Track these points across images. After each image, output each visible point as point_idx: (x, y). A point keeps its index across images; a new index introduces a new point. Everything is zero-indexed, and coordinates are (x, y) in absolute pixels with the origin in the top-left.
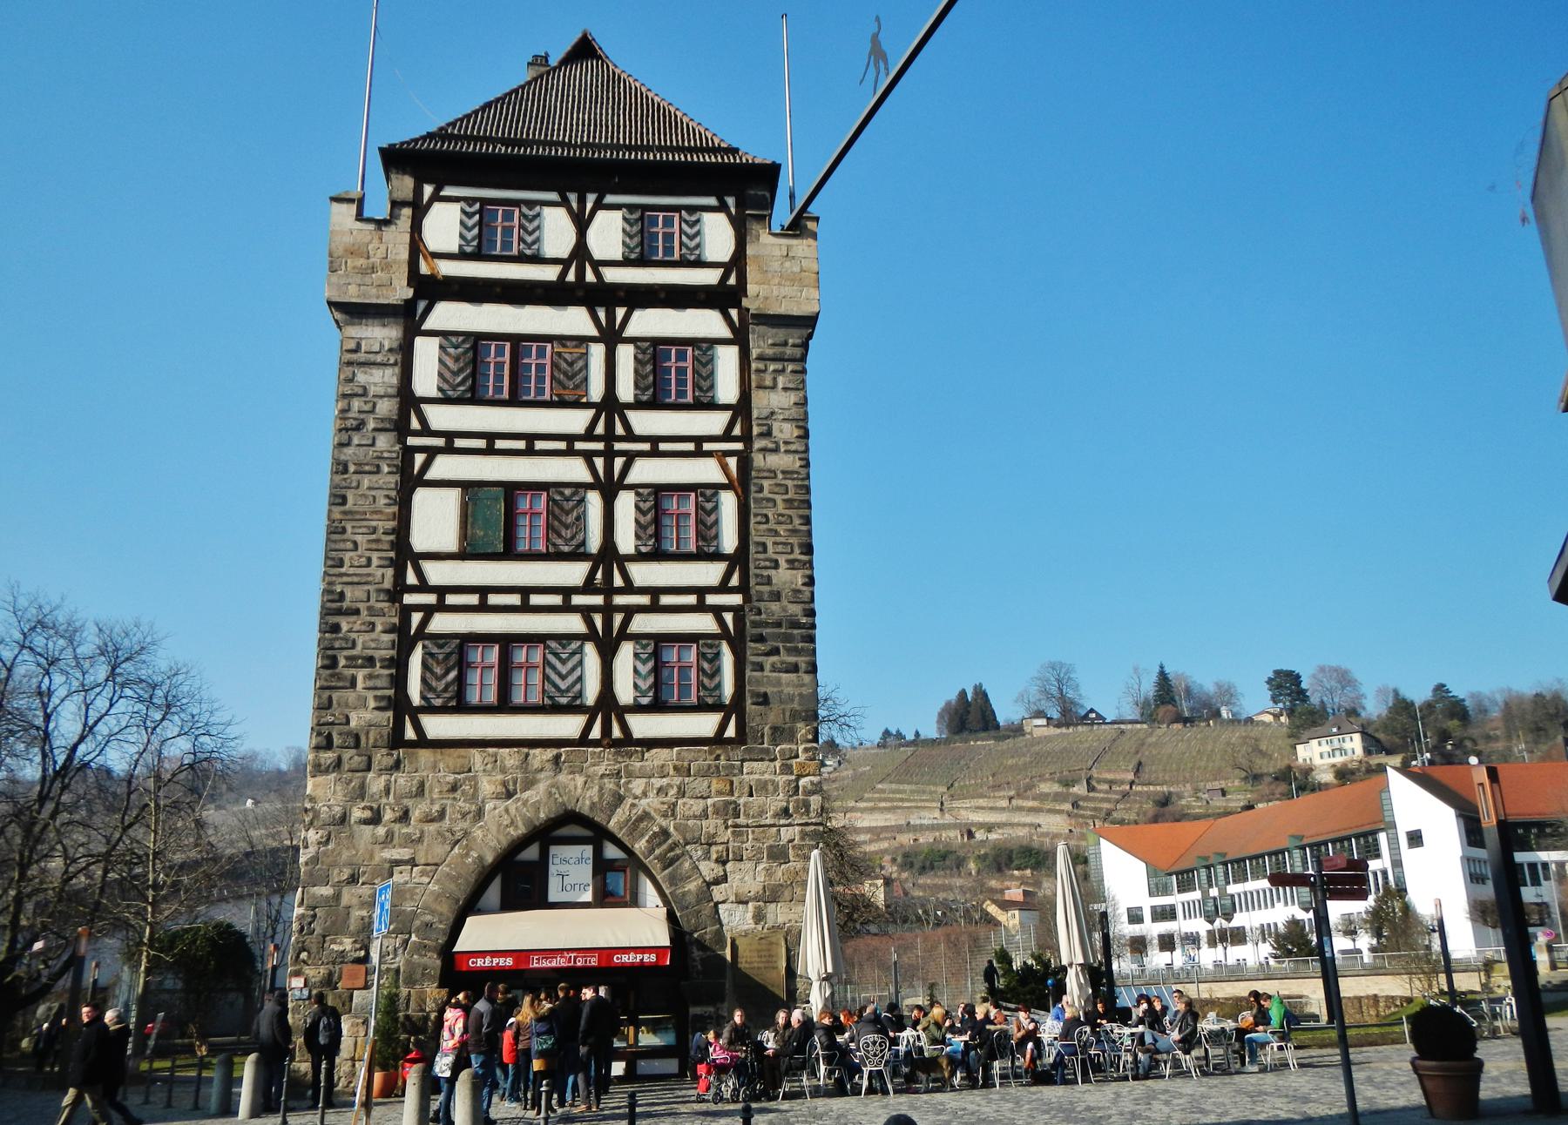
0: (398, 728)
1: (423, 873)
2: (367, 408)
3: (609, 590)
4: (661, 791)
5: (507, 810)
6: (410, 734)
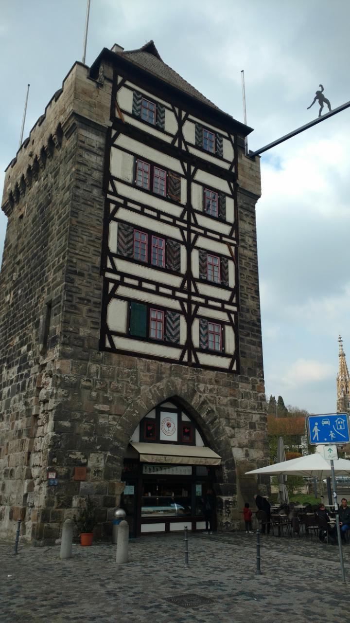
0: (102, 341)
1: (114, 419)
2: (89, 172)
4: (211, 391)
5: (150, 391)
6: (108, 344)
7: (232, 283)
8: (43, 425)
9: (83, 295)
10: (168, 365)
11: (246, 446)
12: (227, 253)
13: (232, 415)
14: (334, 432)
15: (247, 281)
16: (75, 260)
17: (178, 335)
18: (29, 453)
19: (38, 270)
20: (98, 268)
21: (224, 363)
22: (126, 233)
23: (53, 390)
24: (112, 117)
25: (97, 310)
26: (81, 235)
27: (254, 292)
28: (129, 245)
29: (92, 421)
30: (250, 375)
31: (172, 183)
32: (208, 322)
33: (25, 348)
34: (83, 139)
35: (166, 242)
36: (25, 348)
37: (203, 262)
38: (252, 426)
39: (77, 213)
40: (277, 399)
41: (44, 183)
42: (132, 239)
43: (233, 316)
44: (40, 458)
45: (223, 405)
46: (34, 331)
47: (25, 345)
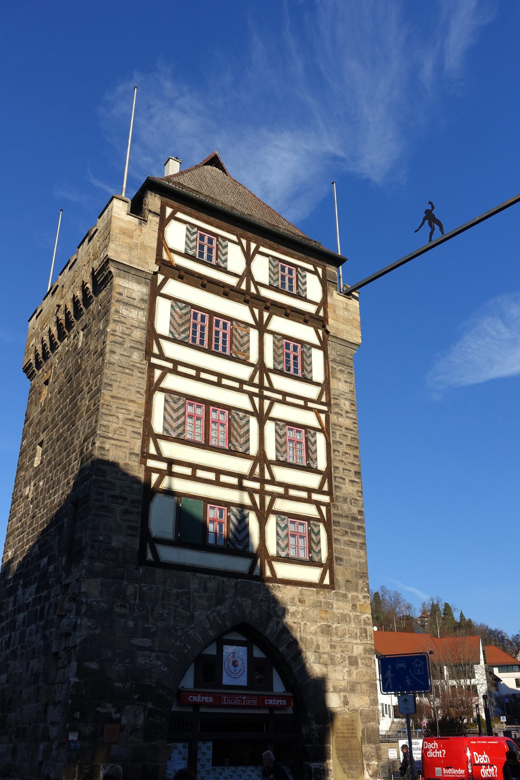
0: (142, 552)
1: (158, 658)
2: (127, 332)
3: (262, 481)
6: (150, 556)
7: (322, 464)
8: (64, 667)
9: (117, 492)
10: (233, 582)
11: (344, 690)
12: (315, 424)
13: (324, 648)
14: (411, 677)
15: (343, 459)
16: (107, 446)
17: (247, 539)
18: (46, 705)
19: (63, 456)
20: (137, 455)
21: (312, 574)
22: (176, 406)
23: (77, 620)
24: (159, 260)
25: (135, 510)
26: (116, 414)
27: (354, 474)
28: (180, 421)
29: (127, 661)
30: (348, 589)
31: (238, 337)
32: (289, 519)
33: (45, 560)
34: (121, 291)
35: (230, 414)
36: (45, 560)
37: (281, 438)
38: (353, 662)
39: (111, 385)
40: (442, 608)
41: (74, 342)
42: (184, 413)
43: (324, 509)
44: (59, 712)
45: (311, 633)
46: (57, 539)
47: (45, 557)
